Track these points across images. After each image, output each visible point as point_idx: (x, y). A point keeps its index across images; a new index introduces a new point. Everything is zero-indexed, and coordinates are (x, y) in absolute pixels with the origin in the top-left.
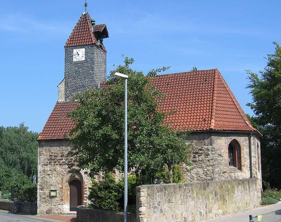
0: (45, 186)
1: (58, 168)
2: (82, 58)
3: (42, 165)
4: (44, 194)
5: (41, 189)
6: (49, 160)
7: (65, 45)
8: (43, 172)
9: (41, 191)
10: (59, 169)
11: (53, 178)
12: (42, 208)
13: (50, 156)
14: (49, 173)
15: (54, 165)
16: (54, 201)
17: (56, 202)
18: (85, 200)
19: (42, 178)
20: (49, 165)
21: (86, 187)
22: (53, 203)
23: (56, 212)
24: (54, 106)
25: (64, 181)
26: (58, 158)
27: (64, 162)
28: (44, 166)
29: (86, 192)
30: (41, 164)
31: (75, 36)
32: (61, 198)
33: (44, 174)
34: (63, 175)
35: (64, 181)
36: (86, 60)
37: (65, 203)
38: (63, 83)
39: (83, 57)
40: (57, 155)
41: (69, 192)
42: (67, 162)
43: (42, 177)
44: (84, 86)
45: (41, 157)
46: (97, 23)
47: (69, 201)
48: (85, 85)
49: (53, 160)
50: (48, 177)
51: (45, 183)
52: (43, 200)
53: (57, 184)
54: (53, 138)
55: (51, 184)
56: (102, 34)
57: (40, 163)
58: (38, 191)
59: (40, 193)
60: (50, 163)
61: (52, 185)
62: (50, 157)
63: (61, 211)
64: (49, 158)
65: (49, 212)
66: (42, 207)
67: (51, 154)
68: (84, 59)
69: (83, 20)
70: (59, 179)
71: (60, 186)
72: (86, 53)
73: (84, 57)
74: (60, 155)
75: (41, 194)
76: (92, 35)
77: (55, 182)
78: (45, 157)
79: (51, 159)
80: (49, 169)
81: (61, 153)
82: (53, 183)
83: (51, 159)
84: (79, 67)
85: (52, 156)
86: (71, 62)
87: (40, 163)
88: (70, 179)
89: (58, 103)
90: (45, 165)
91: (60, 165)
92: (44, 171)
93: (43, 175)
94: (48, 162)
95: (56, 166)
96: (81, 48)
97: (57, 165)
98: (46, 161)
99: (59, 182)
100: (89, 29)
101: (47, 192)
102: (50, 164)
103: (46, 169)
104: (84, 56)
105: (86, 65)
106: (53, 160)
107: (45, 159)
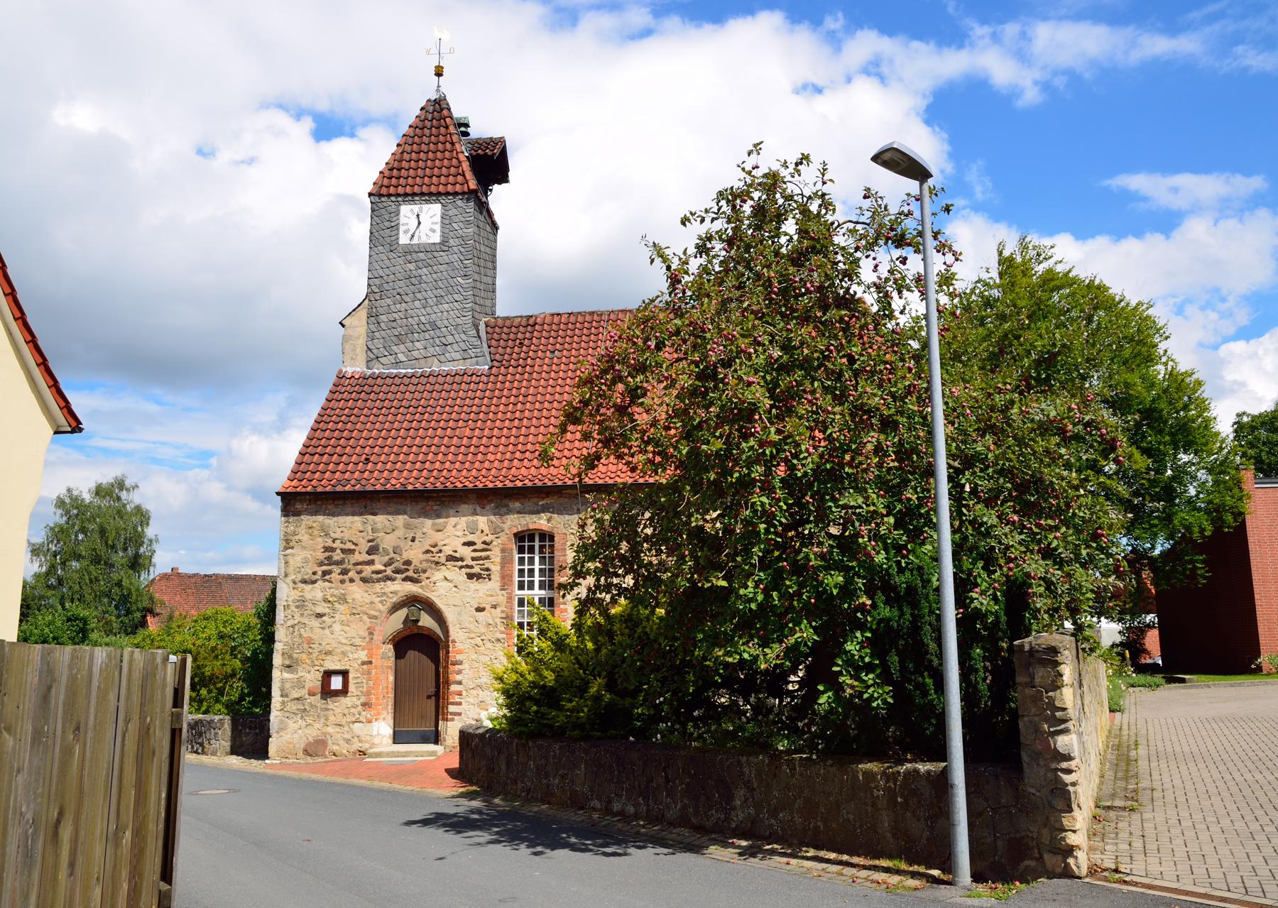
0: (304, 656)
1: (357, 592)
2: (430, 234)
3: (294, 582)
4: (300, 684)
5: (289, 667)
6: (321, 564)
7: (370, 187)
8: (297, 607)
9: (286, 675)
10: (357, 596)
11: (337, 627)
12: (287, 736)
13: (327, 549)
14: (319, 610)
15: (342, 582)
16: (338, 711)
17: (346, 711)
18: (453, 704)
19: (293, 626)
20: (320, 583)
21: (459, 657)
22: (332, 718)
23: (343, 749)
24: (330, 386)
25: (378, 638)
26: (357, 557)
27: (378, 572)
28: (300, 585)
29: (458, 678)
30: (289, 580)
31: (406, 156)
32: (363, 699)
33: (302, 615)
34: (375, 617)
35: (378, 638)
36: (444, 242)
37: (379, 714)
38: (363, 313)
39: (434, 231)
40: (353, 547)
41: (391, 678)
43: (290, 623)
44: (435, 327)
45: (293, 555)
46: (476, 132)
47: (390, 708)
48: (439, 323)
49: (338, 563)
50: (315, 623)
51: (305, 646)
52: (293, 707)
53: (348, 648)
54: (339, 488)
55: (328, 648)
56: (491, 164)
57: (286, 576)
58: (276, 674)
59: (283, 681)
60: (325, 573)
61: (328, 653)
62: (327, 554)
63: (365, 746)
64: (321, 556)
65: (314, 749)
66: (288, 729)
67: (329, 543)
68: (436, 238)
69: (430, 117)
70: (358, 630)
71: (363, 656)
72: (446, 220)
73: (438, 233)
74: (364, 546)
75: (287, 685)
76: (466, 165)
77: (344, 641)
78: (307, 554)
79: (330, 561)
80: (319, 595)
82: (334, 645)
83: (330, 561)
84: (420, 264)
85: (333, 550)
86: (393, 245)
88: (404, 629)
89: (341, 376)
90: (304, 582)
91: (364, 580)
92: (301, 604)
93: (298, 618)
94: (320, 570)
96: (427, 202)
97: (352, 581)
98: (309, 570)
99: (358, 641)
100: (453, 144)
101: (313, 679)
103: (308, 596)
104: (438, 228)
105: (444, 257)
106: (338, 563)
107: (306, 561)
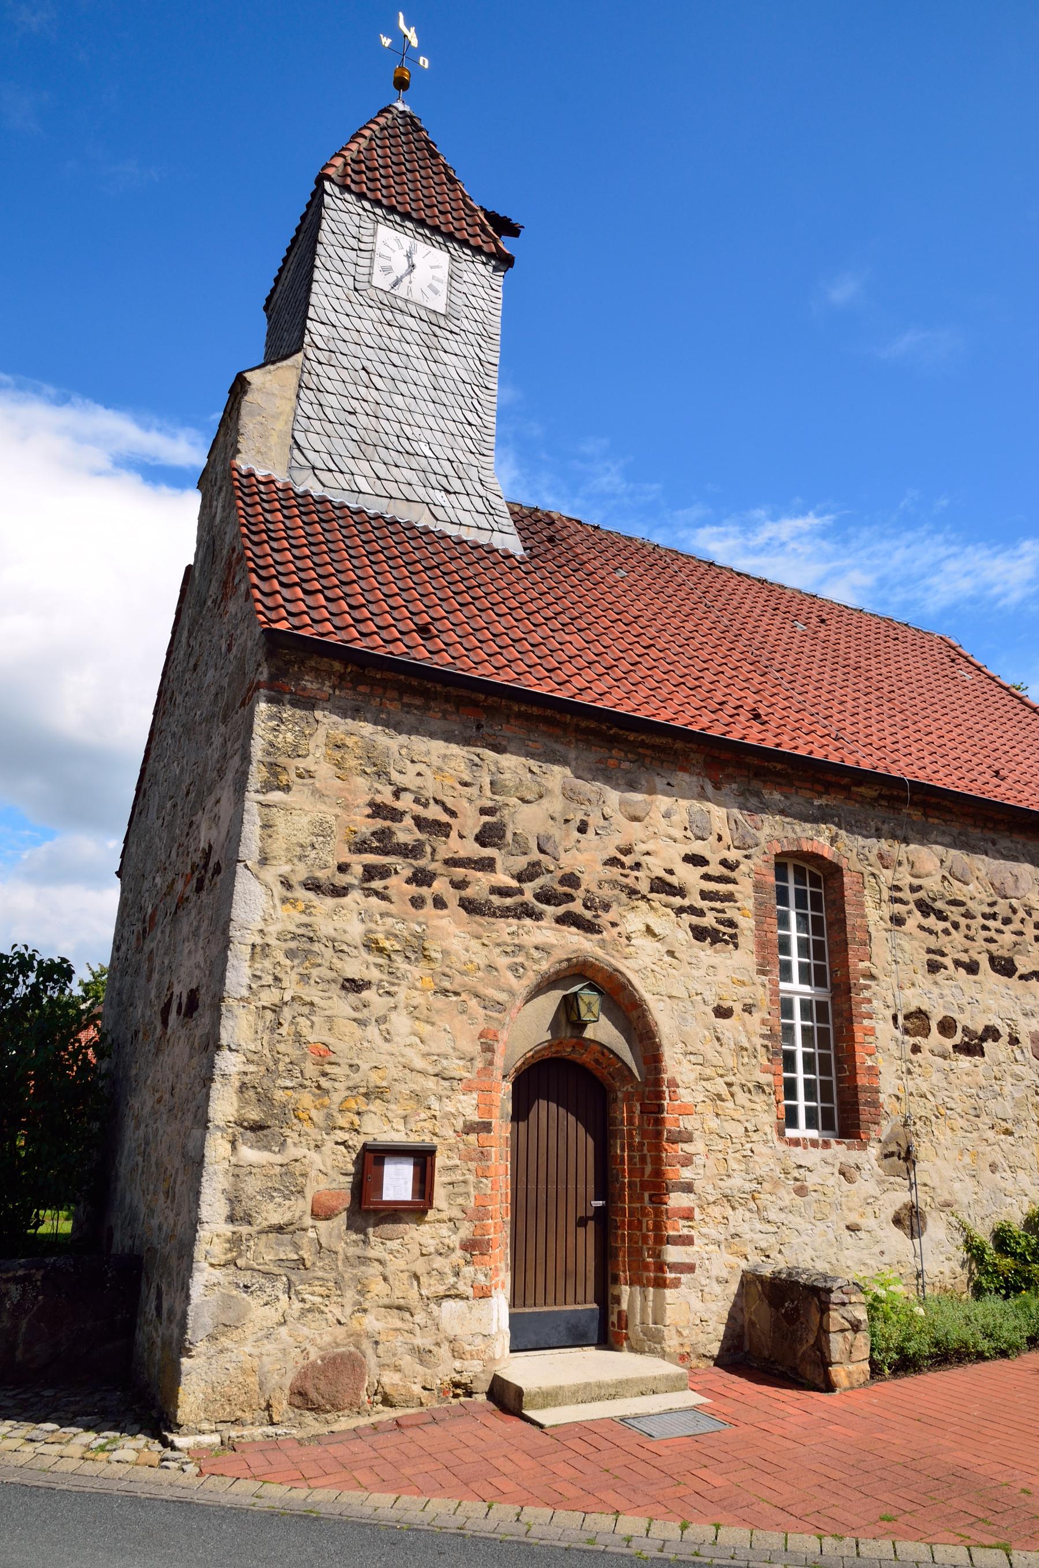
4: (289, 1182)
5: (257, 1127)
9: (249, 1154)
13: (378, 810)
15: (417, 902)
40: (445, 818)
42: (528, 897)
45: (288, 809)
58: (217, 1149)
59: (238, 1172)
62: (379, 824)
64: (366, 827)
74: (472, 822)
75: (252, 1186)
81: (484, 811)
87: (264, 861)
90: (314, 886)
92: (304, 944)
94: (358, 862)
95: (429, 907)
97: (439, 903)
99: (455, 1067)
102: (377, 884)
107: (322, 830)
